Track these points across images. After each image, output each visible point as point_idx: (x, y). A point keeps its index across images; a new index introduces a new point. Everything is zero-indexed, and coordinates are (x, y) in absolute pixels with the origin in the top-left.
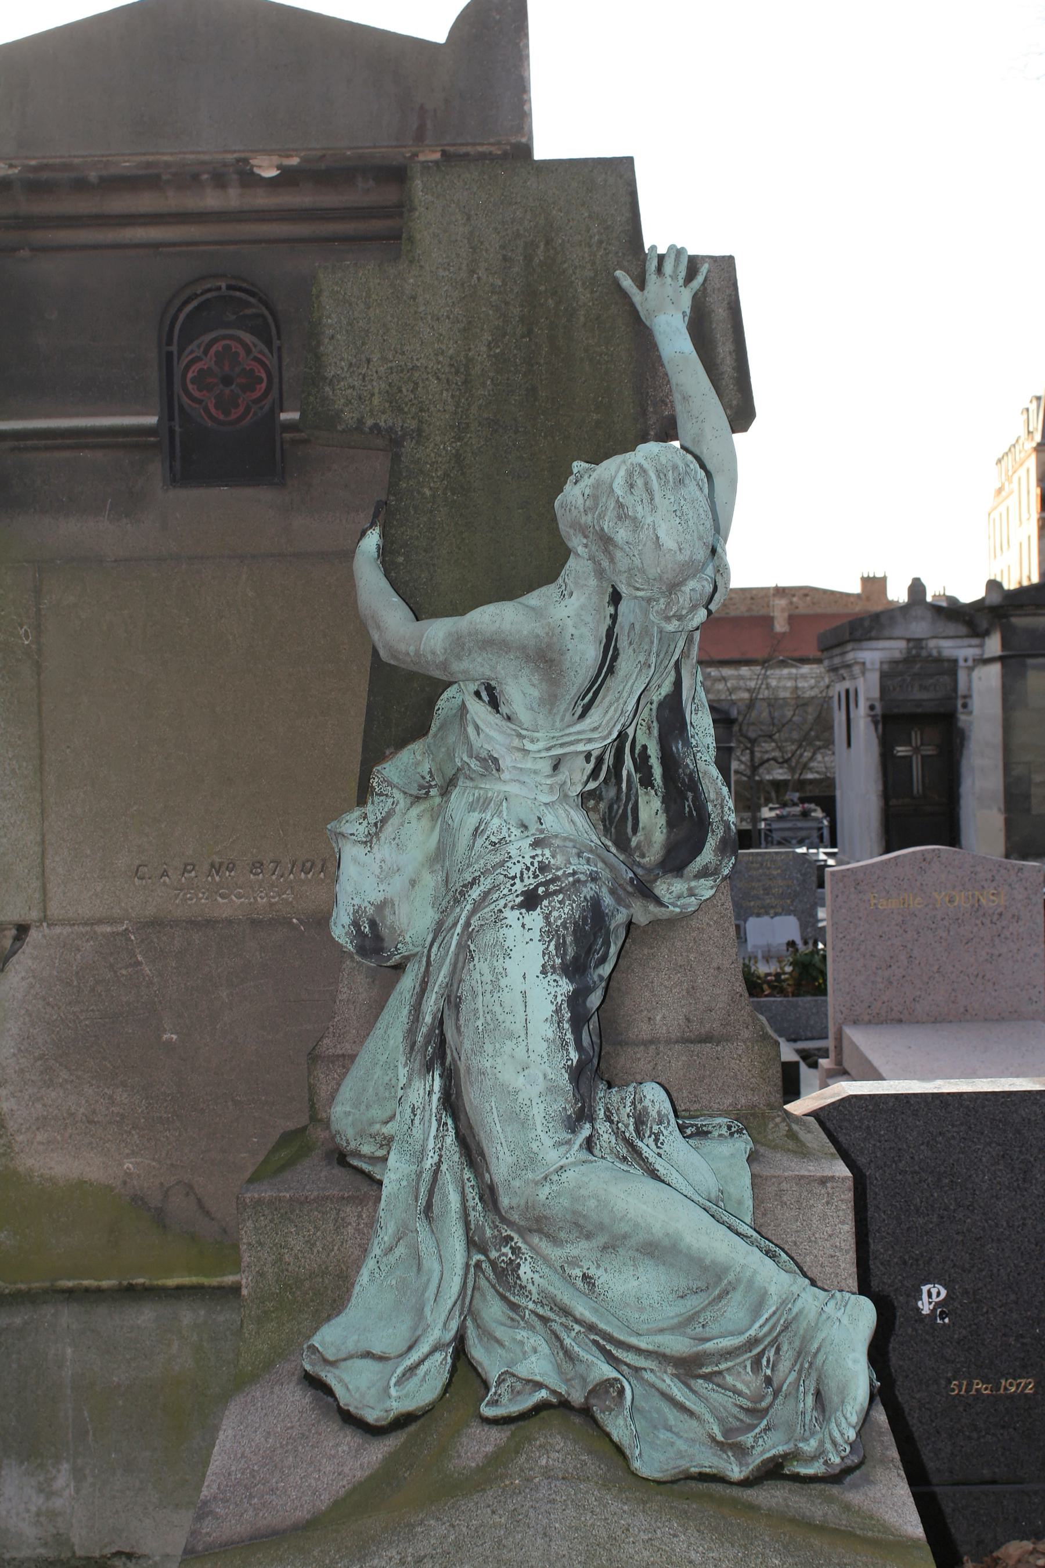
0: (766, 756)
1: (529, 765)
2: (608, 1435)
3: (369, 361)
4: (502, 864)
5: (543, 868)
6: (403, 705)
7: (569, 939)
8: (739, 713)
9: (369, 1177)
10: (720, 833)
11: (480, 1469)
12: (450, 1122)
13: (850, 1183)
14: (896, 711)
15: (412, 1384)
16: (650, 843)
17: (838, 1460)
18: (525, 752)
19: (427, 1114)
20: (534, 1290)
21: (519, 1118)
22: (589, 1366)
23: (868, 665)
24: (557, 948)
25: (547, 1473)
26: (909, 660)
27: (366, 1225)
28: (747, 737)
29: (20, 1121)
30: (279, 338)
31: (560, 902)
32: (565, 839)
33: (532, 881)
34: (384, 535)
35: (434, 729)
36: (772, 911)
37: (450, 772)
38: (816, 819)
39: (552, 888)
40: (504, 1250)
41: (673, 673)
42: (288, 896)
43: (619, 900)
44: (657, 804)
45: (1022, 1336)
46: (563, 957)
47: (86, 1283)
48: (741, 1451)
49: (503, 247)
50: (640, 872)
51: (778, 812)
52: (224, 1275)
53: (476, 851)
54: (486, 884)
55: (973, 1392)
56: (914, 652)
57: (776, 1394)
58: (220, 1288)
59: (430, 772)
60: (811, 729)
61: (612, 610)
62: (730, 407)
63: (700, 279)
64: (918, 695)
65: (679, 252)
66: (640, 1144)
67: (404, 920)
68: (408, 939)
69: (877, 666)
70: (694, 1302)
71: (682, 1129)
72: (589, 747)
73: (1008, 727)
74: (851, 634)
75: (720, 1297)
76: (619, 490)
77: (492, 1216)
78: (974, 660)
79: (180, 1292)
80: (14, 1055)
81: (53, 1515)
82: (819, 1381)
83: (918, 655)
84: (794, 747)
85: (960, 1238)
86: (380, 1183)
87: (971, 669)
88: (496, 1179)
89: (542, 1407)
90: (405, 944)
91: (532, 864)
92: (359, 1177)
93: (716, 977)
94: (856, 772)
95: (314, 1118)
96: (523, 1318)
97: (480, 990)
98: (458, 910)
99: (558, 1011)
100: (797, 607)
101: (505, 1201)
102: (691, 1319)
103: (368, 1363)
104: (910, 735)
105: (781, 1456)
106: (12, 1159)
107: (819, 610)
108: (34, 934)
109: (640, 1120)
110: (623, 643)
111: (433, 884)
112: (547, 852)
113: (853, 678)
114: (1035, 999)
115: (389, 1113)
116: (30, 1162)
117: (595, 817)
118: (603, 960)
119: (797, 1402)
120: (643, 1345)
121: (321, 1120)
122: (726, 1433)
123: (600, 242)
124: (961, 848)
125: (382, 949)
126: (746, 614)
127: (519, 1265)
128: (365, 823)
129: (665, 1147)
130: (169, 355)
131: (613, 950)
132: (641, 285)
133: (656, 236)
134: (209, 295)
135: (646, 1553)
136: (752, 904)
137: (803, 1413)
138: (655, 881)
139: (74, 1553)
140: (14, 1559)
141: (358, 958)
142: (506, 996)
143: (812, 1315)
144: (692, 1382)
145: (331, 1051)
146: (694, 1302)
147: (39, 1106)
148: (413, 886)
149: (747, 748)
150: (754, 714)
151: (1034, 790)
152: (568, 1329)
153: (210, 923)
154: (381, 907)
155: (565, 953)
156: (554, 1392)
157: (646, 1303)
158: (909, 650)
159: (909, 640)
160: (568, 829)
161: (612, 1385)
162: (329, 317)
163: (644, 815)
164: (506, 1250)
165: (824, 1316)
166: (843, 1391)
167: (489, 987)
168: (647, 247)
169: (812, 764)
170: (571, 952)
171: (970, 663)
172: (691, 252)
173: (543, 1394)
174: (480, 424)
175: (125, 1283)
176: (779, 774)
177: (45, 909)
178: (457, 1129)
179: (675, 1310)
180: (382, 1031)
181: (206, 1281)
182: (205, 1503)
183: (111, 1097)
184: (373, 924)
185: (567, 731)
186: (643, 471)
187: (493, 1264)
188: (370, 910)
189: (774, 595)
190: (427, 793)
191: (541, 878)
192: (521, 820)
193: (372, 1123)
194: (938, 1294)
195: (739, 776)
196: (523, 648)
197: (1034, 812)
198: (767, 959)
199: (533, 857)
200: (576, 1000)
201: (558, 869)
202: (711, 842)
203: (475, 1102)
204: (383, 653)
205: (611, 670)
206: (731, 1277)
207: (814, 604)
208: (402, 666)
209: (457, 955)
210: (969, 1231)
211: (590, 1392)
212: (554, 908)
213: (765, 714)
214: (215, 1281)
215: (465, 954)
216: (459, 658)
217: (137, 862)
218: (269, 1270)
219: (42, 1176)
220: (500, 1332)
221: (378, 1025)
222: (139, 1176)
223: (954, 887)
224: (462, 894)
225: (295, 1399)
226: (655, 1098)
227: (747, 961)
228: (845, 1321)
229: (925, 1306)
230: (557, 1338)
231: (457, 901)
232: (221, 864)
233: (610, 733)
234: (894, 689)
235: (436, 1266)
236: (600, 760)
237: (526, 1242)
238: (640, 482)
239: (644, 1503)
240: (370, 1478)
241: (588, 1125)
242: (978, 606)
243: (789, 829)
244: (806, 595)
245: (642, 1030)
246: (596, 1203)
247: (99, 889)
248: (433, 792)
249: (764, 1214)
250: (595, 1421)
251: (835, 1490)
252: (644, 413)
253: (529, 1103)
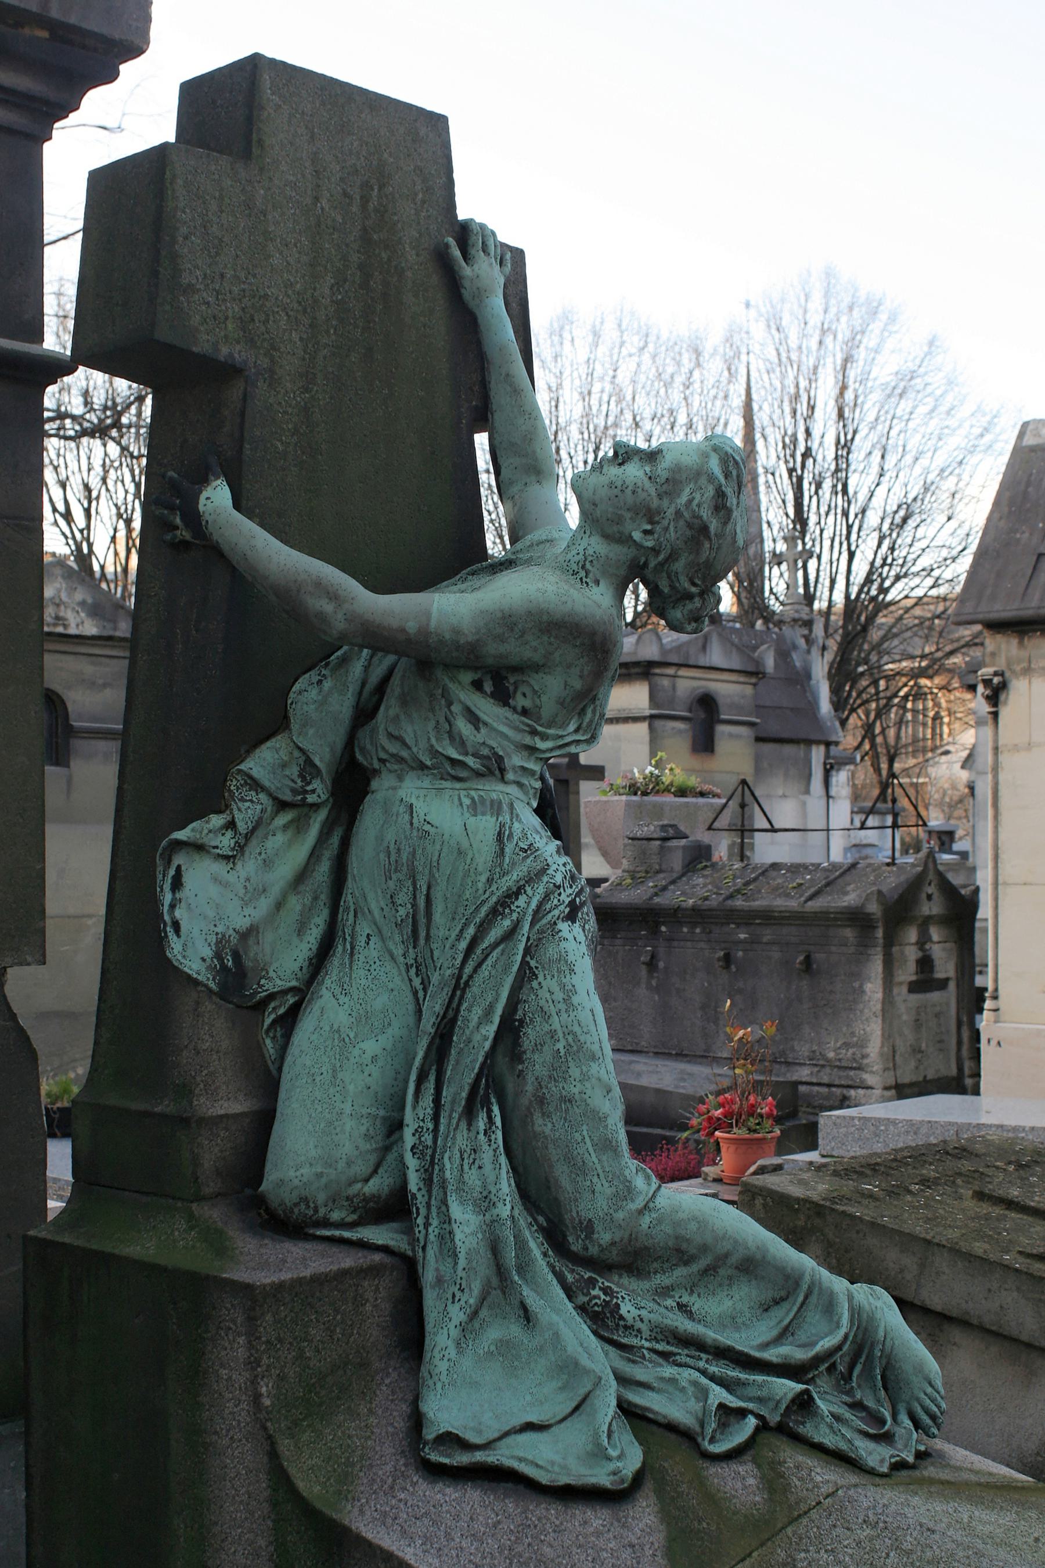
20: (644, 1327)
40: (594, 1293)
68: (272, 974)
90: (270, 979)
111: (298, 908)
127: (617, 1306)
148: (278, 911)
154: (247, 934)
157: (739, 1321)
164: (595, 1292)
167: (562, 1006)
184: (236, 956)
246: (697, 1225)
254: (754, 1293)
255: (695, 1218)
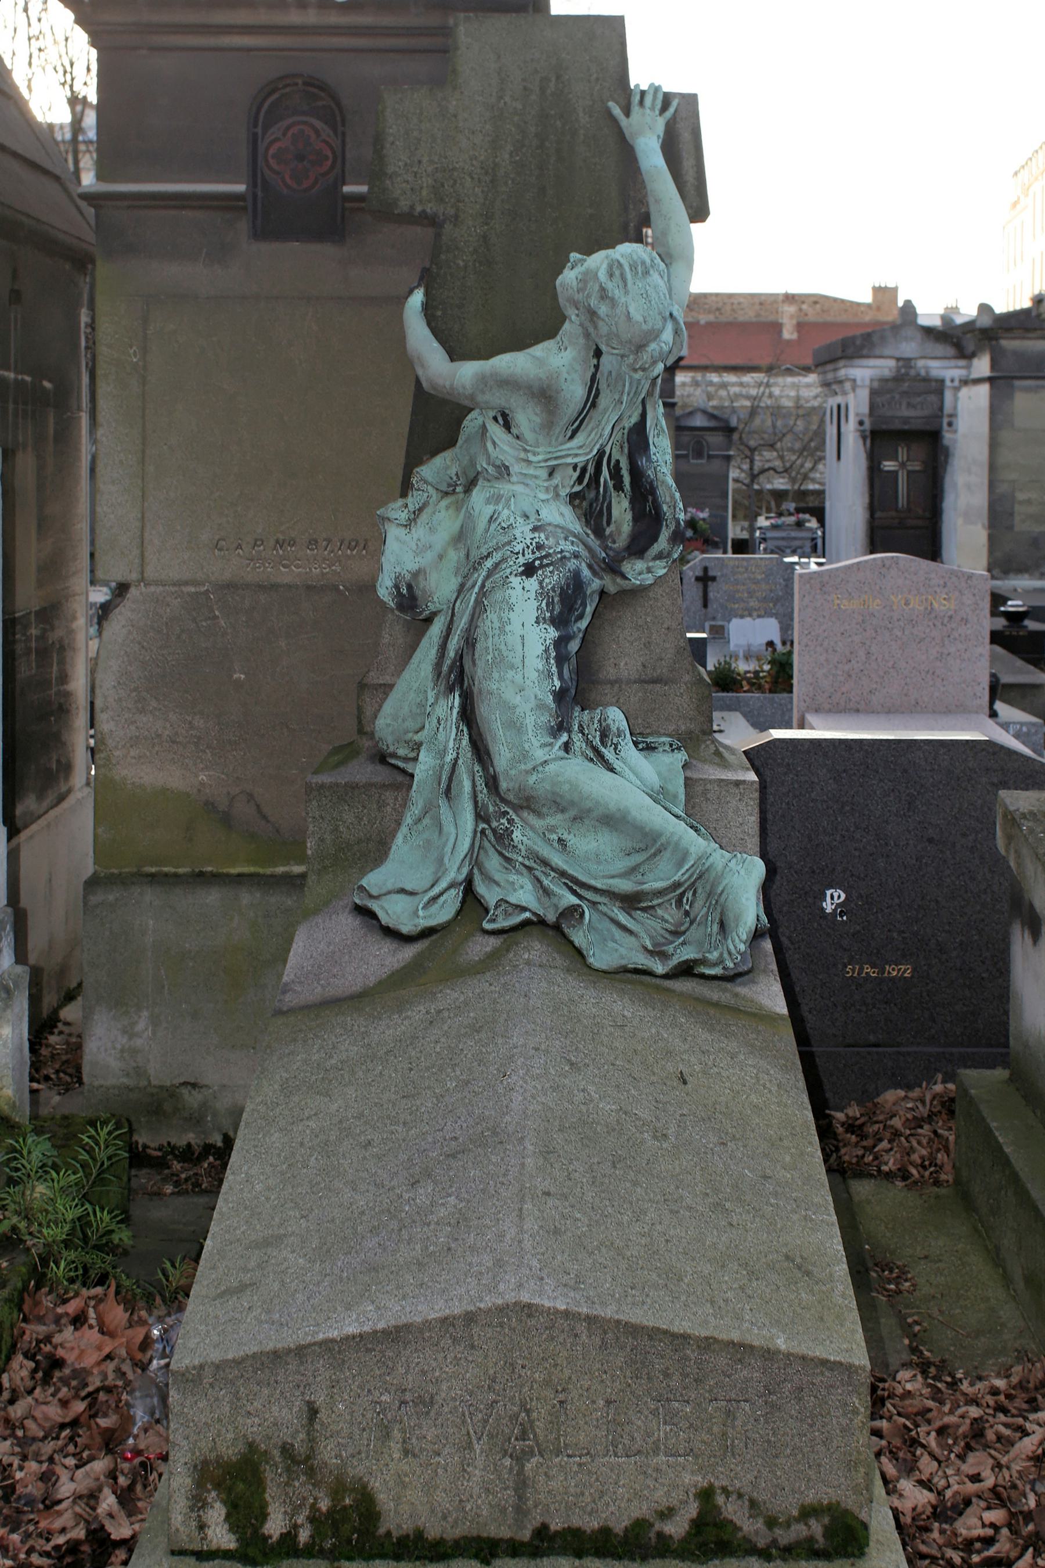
0: (766, 466)
1: (531, 472)
2: (572, 943)
3: (420, 162)
4: (509, 543)
5: (539, 547)
6: (437, 423)
7: (556, 599)
8: (739, 419)
9: (403, 771)
10: (673, 527)
11: (481, 961)
12: (465, 729)
13: (757, 786)
14: (884, 427)
15: (434, 908)
16: (620, 533)
17: (732, 965)
18: (528, 462)
19: (449, 723)
20: (523, 848)
21: (515, 726)
22: (560, 897)
23: (859, 382)
24: (547, 605)
25: (528, 963)
26: (898, 378)
27: (401, 805)
28: (747, 446)
29: (117, 739)
30: (343, 125)
32: (557, 526)
33: (531, 556)
34: (427, 294)
35: (460, 442)
36: (755, 614)
37: (472, 475)
38: (810, 529)
39: (545, 561)
40: (502, 821)
41: (640, 407)
42: (337, 568)
43: (595, 573)
44: (626, 504)
45: (903, 932)
46: (552, 612)
47: (166, 869)
48: (663, 956)
49: (524, 80)
50: (611, 553)
51: (773, 521)
52: (276, 866)
53: (497, 530)
54: (497, 557)
55: (864, 975)
56: (903, 371)
57: (692, 923)
58: (272, 876)
59: (457, 474)
60: (811, 440)
61: (595, 361)
62: (691, 207)
63: (672, 110)
64: (906, 412)
65: (657, 89)
66: (603, 750)
67: (433, 585)
68: (435, 599)
69: (867, 382)
70: (638, 858)
71: (636, 744)
72: (576, 460)
73: (994, 445)
74: (843, 351)
75: (655, 855)
76: (602, 275)
77: (494, 798)
78: (960, 381)
79: (240, 879)
80: (114, 687)
81: (134, 1052)
82: (722, 914)
83: (907, 374)
84: (794, 458)
85: (857, 853)
86: (412, 776)
87: (957, 389)
88: (498, 769)
89: (526, 923)
90: (434, 602)
92: (396, 771)
93: (666, 635)
94: (845, 484)
95: (361, 731)
96: (514, 868)
97: (491, 634)
98: (476, 575)
99: (546, 650)
100: (806, 315)
101: (504, 785)
102: (634, 869)
103: (402, 897)
104: (897, 451)
105: (691, 961)
106: (110, 770)
107: (829, 318)
108: (133, 592)
109: (604, 734)
110: (603, 386)
111: (456, 558)
112: (542, 536)
113: (845, 393)
114: (978, 694)
115: (419, 725)
116: (124, 772)
117: (579, 512)
118: (581, 617)
119: (706, 927)
120: (599, 886)
121: (366, 733)
122: (654, 945)
123: (597, 79)
124: (942, 562)
125: (416, 606)
126: (754, 320)
128: (406, 511)
129: (622, 753)
130: (255, 135)
131: (589, 610)
132: (627, 113)
133: (639, 77)
134: (288, 90)
135: (594, 1010)
136: (736, 606)
137: (710, 935)
138: (623, 561)
139: (150, 1081)
140: (102, 1086)
141: (397, 613)
142: (509, 638)
143: (720, 868)
144: (633, 913)
145: (376, 681)
146: (638, 858)
147: (133, 728)
149: (746, 457)
150: (757, 422)
151: (1017, 508)
152: (547, 875)
153: (274, 587)
154: (416, 574)
155: (553, 610)
156: (534, 914)
157: (602, 858)
158: (898, 369)
159: (898, 359)
160: (558, 520)
161: (576, 910)
162: (391, 127)
163: (615, 512)
164: (504, 821)
165: (728, 869)
166: (737, 919)
167: (497, 632)
168: (632, 87)
169: (812, 475)
170: (557, 609)
171: (956, 383)
172: (665, 89)
173: (527, 915)
174: (502, 213)
175: (197, 870)
176: (780, 483)
177: (142, 573)
178: (470, 735)
179: (623, 864)
180: (415, 666)
181: (261, 871)
182: (286, 984)
183: (190, 723)
184: (410, 587)
185: (560, 448)
186: (620, 265)
187: (494, 831)
188: (408, 577)
189: (783, 301)
190: (454, 490)
191: (538, 555)
193: (406, 732)
194: (839, 897)
195: (739, 485)
196: (530, 387)
197: (1017, 529)
198: (747, 658)
200: (560, 643)
201: (550, 548)
202: (665, 535)
203: (485, 715)
204: (425, 384)
205: (594, 405)
206: (663, 840)
207: (823, 311)
208: (440, 395)
209: (474, 608)
210: (865, 848)
211: (561, 914)
212: (546, 576)
213: (769, 423)
214: (269, 871)
215: (480, 608)
216: (483, 392)
217: (217, 537)
218: (328, 837)
219: (133, 783)
220: (497, 877)
221: (412, 661)
222: (211, 786)
223: (910, 591)
224: (480, 564)
225: (347, 923)
226: (616, 717)
227: (728, 659)
228: (742, 872)
229: (828, 907)
230: (538, 880)
231: (475, 569)
232: (284, 541)
233: (591, 451)
234: (883, 405)
235: (453, 830)
236: (584, 470)
237: (518, 816)
238: (617, 273)
239: (595, 983)
240: (404, 967)
241: (565, 734)
242: (969, 327)
243: (783, 539)
244: (816, 303)
245: (609, 672)
247: (186, 557)
248: (459, 489)
249: (693, 807)
250: (564, 936)
251: (729, 985)
252: (626, 209)
254: (615, 841)
255: (569, 782)
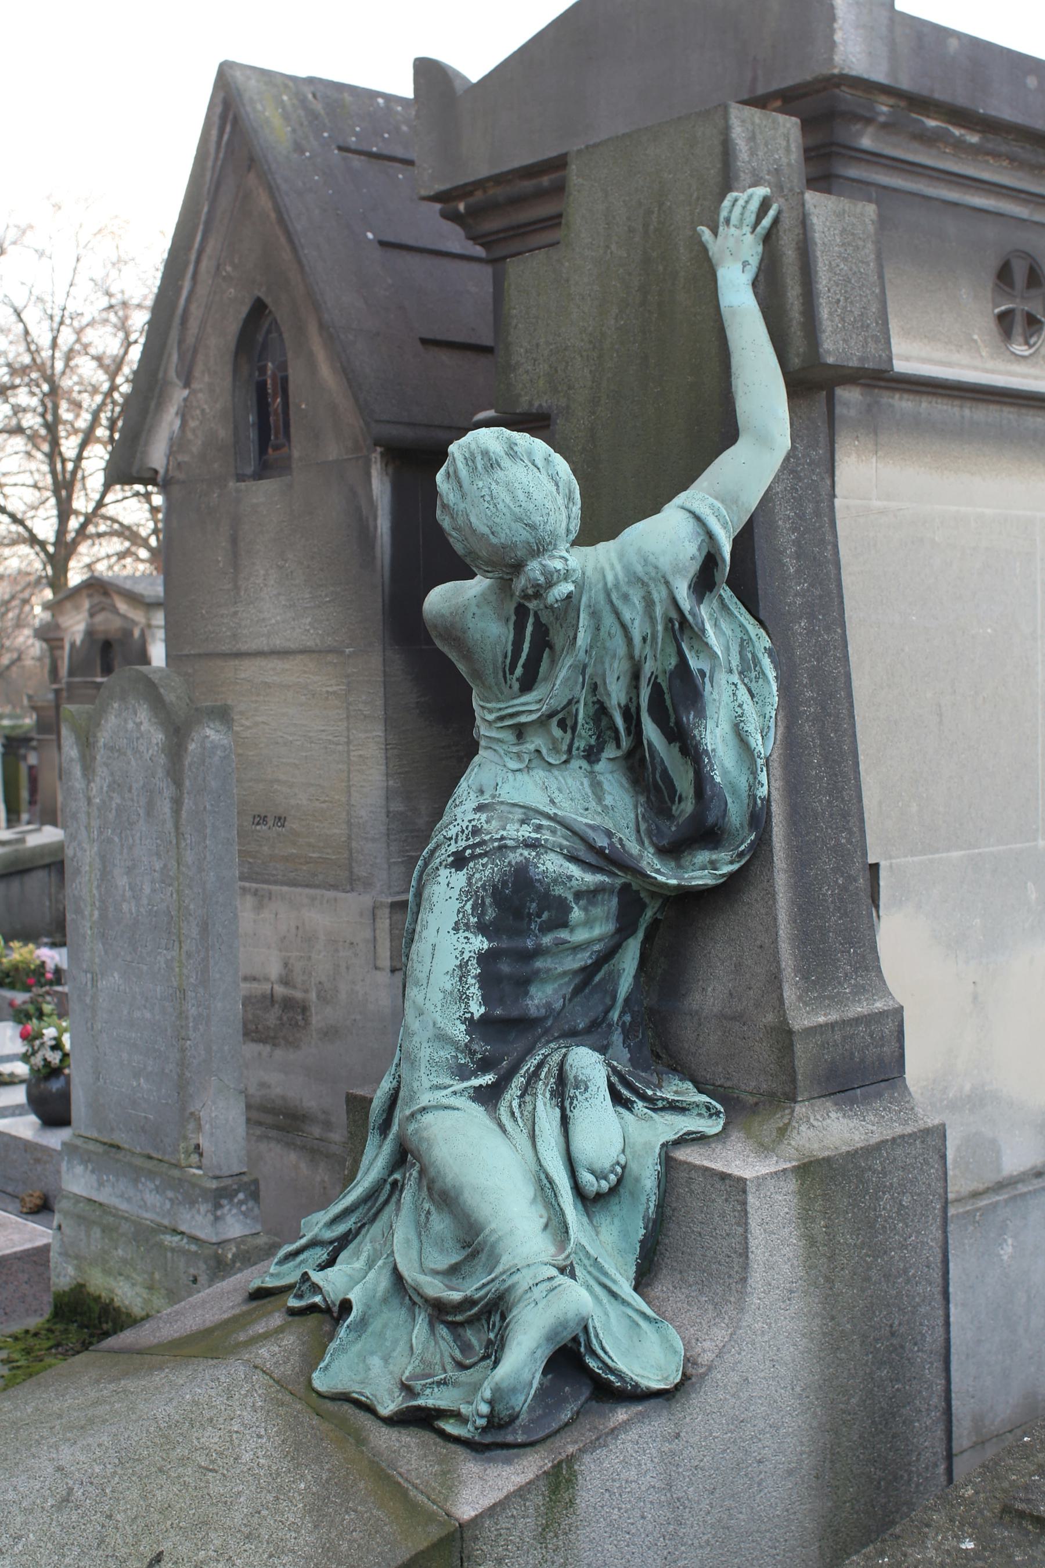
5: (476, 831)
7: (488, 901)
24: (473, 908)
31: (483, 865)
39: (478, 851)
46: (480, 917)
89: (313, 1308)
91: (467, 827)
93: (758, 955)
99: (463, 966)
123: (698, 199)
132: (715, 233)
155: (483, 913)
173: (317, 1299)
185: (511, 703)
192: (481, 786)
199: (470, 821)
212: (477, 870)
253: (418, 1045)
